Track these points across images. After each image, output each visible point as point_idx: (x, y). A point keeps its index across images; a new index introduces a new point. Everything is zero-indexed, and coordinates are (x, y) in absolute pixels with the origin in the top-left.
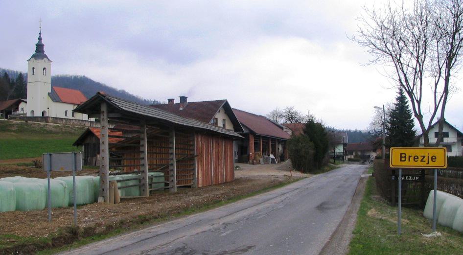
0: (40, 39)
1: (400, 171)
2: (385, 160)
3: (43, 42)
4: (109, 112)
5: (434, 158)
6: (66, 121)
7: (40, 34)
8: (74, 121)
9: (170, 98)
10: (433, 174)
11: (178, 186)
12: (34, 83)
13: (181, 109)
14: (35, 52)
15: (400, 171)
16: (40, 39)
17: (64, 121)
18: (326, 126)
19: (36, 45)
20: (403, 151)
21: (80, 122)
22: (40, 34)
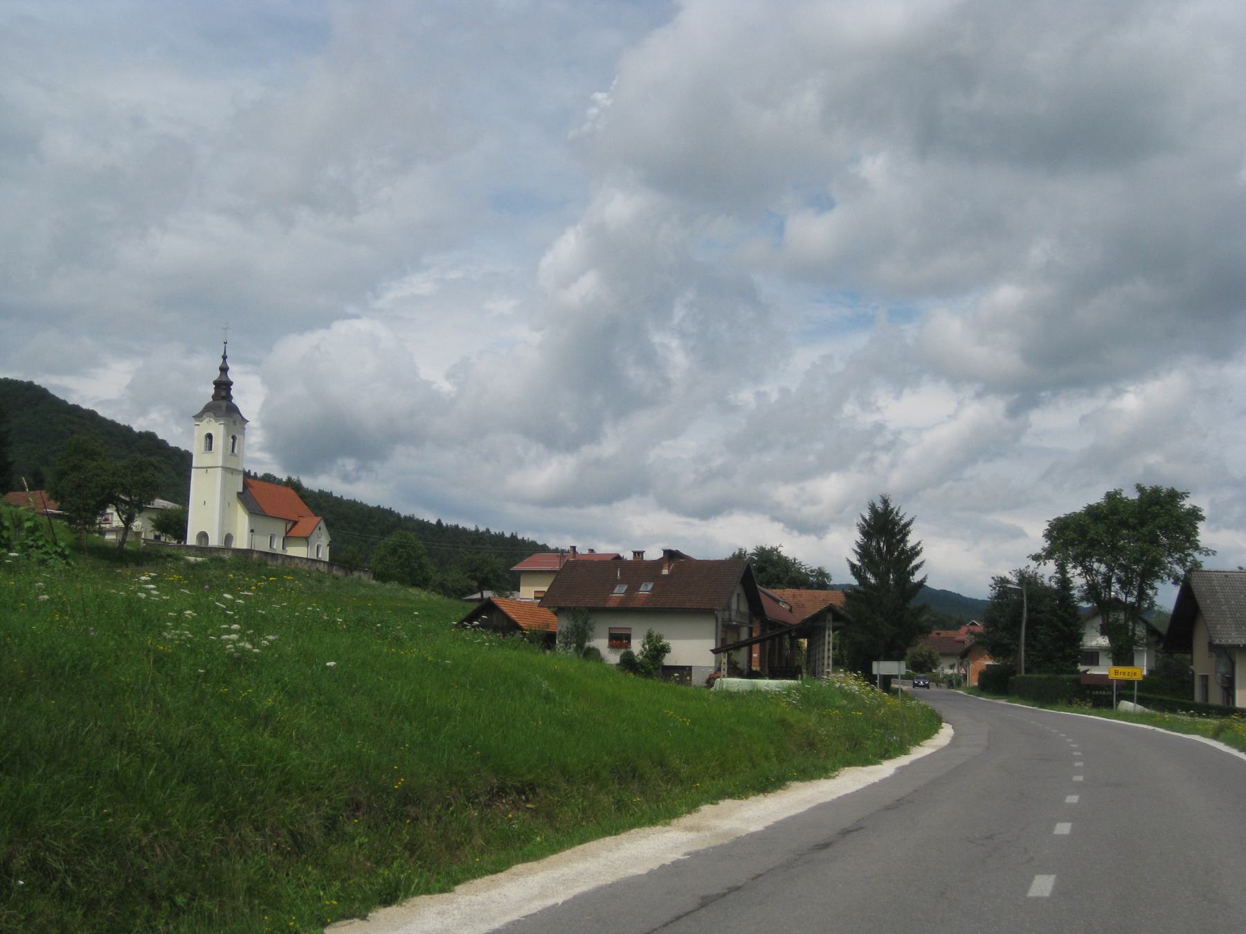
0: (224, 370)
1: (1136, 683)
2: (839, 650)
3: (231, 376)
4: (835, 620)
5: (1135, 674)
6: (283, 561)
7: (225, 357)
8: (297, 561)
9: (636, 550)
10: (1133, 688)
11: (1140, 694)
12: (209, 470)
13: (665, 572)
14: (212, 400)
15: (1136, 683)
16: (224, 370)
17: (280, 561)
18: (370, 506)
19: (215, 383)
20: (1117, 669)
21: (310, 562)
22: (225, 357)
